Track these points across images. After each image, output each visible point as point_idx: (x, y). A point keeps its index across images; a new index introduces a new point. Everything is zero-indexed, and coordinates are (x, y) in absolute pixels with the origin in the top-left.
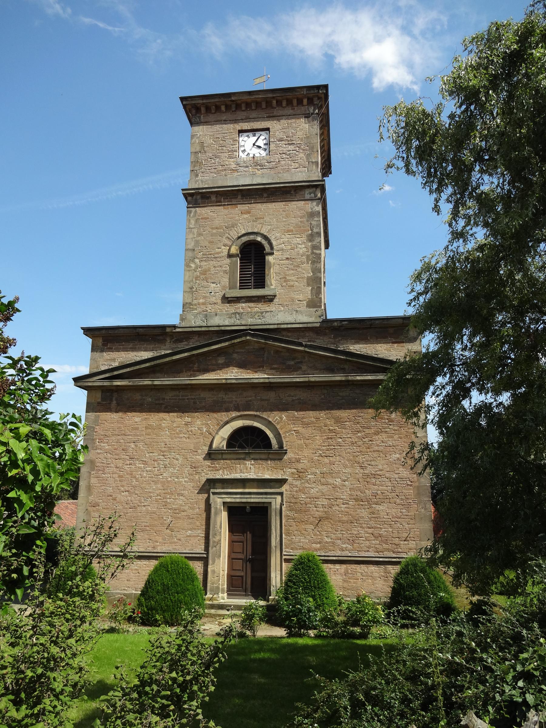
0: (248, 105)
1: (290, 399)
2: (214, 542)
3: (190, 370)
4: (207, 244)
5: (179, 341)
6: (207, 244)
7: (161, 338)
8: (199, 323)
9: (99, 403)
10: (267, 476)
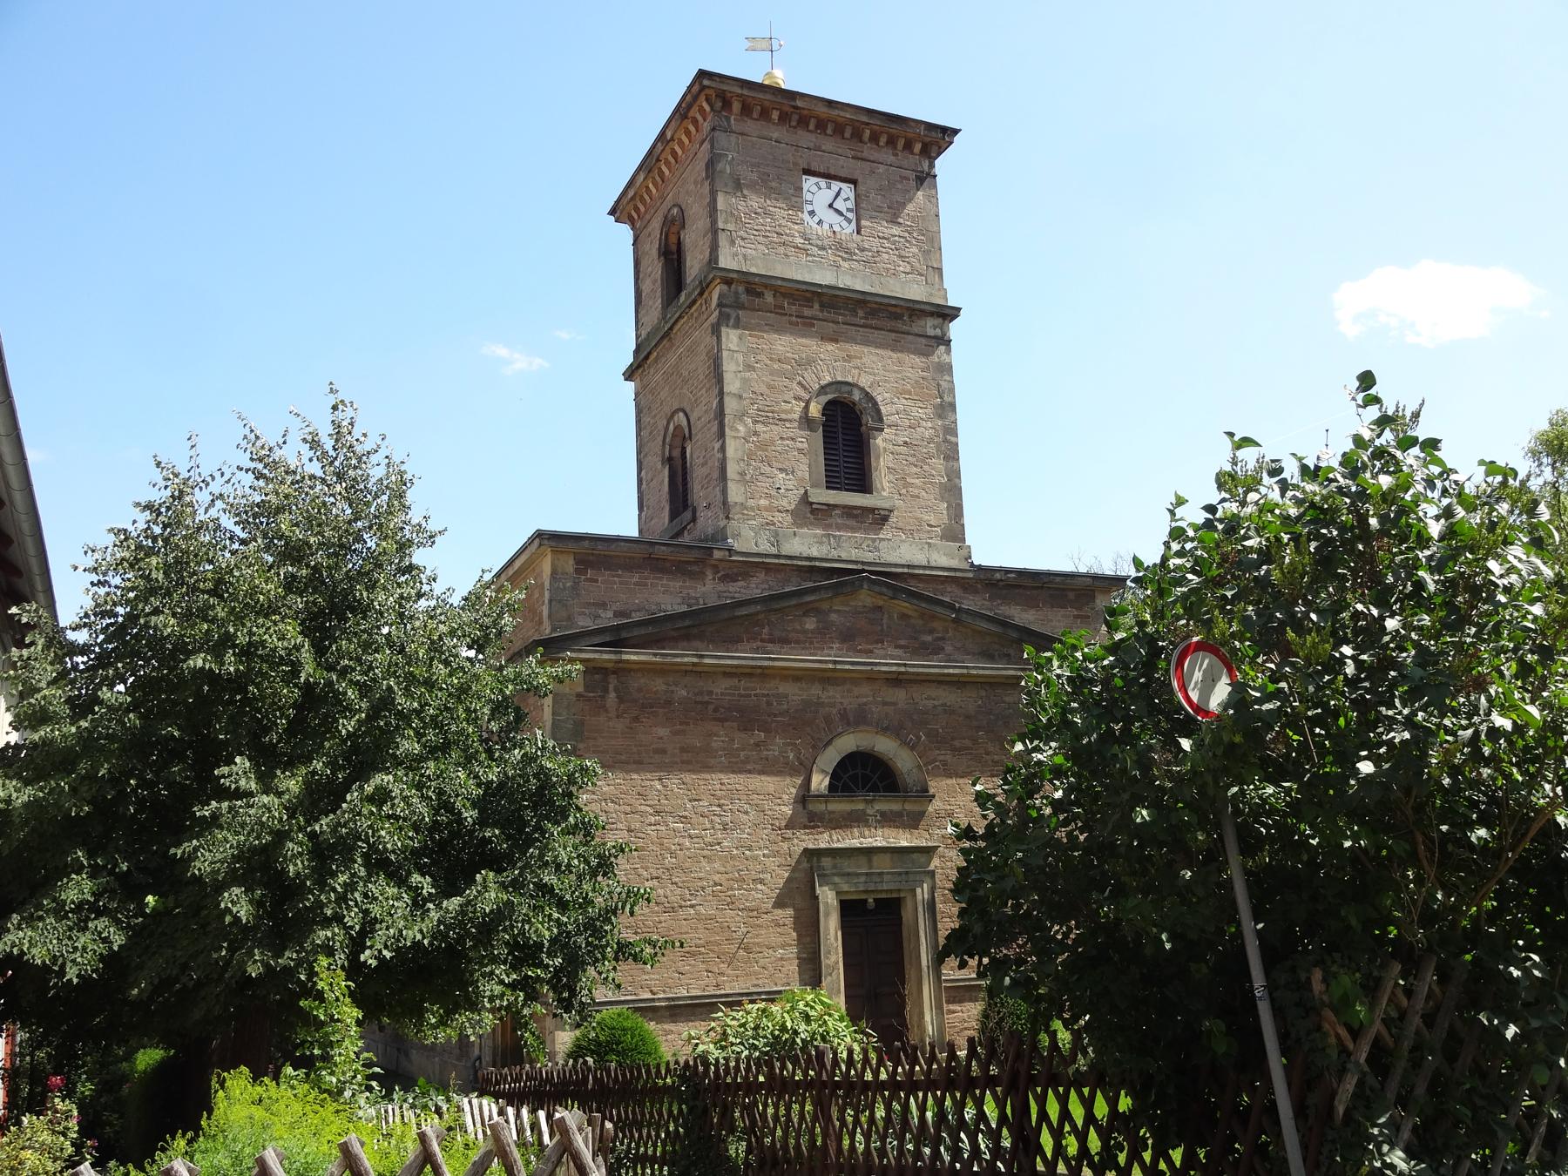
0: (821, 125)
1: (930, 703)
2: (828, 966)
3: (755, 639)
4: (764, 389)
5: (729, 578)
6: (764, 389)
7: (695, 568)
8: (765, 547)
9: (579, 695)
10: (904, 844)
